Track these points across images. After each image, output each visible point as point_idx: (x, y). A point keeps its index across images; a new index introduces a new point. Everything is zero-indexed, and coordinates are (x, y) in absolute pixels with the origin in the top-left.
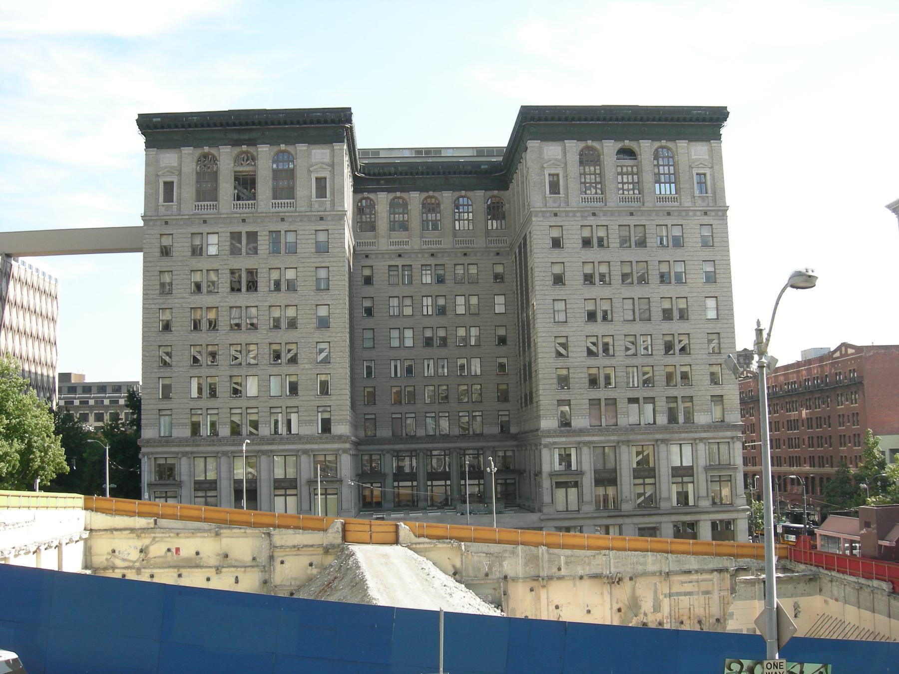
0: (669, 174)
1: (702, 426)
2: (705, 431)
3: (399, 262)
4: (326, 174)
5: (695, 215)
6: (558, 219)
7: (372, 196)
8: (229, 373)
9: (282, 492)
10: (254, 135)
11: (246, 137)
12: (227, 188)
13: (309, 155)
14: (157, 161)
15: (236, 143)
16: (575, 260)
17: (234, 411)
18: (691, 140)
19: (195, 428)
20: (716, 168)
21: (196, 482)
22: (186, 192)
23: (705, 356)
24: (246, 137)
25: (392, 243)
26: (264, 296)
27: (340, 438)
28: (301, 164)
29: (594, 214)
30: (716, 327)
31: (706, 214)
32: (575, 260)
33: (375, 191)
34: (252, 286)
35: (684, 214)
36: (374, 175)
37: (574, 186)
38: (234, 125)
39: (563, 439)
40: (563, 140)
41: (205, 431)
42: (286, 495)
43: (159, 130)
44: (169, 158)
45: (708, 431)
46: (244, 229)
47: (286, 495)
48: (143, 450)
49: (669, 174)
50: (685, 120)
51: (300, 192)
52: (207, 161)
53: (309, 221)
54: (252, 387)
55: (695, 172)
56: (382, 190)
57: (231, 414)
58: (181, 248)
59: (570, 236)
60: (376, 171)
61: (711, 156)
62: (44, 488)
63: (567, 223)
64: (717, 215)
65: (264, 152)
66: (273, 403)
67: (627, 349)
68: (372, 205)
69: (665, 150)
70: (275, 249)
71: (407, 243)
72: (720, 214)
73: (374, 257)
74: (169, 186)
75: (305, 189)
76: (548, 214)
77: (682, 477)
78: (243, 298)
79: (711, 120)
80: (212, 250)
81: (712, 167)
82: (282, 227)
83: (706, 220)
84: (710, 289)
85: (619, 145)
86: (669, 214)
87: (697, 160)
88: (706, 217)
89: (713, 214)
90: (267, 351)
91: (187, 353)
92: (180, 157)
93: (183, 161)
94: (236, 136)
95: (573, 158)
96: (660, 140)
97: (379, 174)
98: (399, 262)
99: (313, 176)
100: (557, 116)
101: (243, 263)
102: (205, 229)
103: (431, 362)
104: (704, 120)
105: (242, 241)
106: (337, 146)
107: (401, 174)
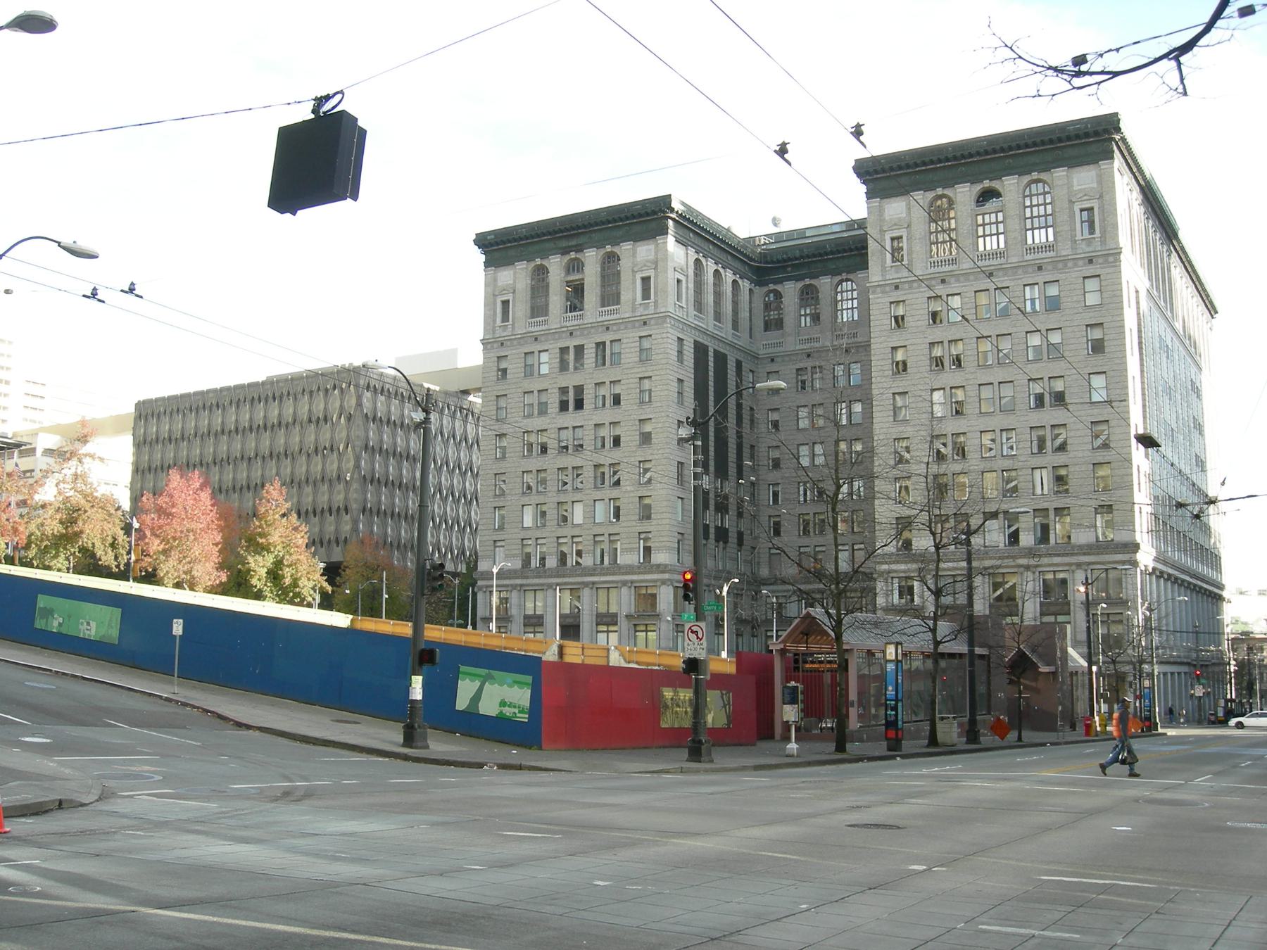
0: (1046, 215)
1: (1080, 547)
2: (1085, 554)
3: (809, 364)
4: (651, 273)
5: (1076, 265)
6: (899, 292)
7: (779, 287)
8: (556, 500)
9: (605, 628)
10: (582, 240)
11: (574, 243)
12: (556, 300)
13: (634, 255)
14: (495, 280)
15: (565, 252)
16: (919, 341)
17: (561, 540)
18: (1071, 167)
19: (527, 560)
20: (1106, 197)
21: (526, 617)
22: (520, 309)
23: (1087, 453)
24: (574, 243)
25: (802, 342)
26: (589, 416)
27: (661, 568)
28: (625, 265)
29: (943, 281)
30: (1105, 413)
31: (1091, 261)
32: (919, 341)
33: (780, 281)
34: (579, 405)
35: (1060, 265)
36: (779, 262)
37: (919, 249)
38: (562, 231)
39: (903, 567)
40: (907, 193)
41: (535, 563)
42: (608, 632)
43: (500, 247)
44: (506, 276)
45: (1089, 554)
46: (571, 343)
47: (647, 631)
48: (480, 583)
49: (1046, 215)
50: (1060, 140)
51: (625, 297)
52: (541, 272)
53: (634, 327)
54: (578, 515)
55: (1077, 208)
56: (789, 279)
57: (559, 544)
58: (514, 366)
59: (914, 313)
60: (780, 257)
61: (1100, 182)
62: (135, 580)
63: (910, 296)
64: (1106, 261)
65: (592, 258)
66: (597, 531)
67: (908, 449)
68: (778, 296)
69: (1040, 185)
70: (601, 361)
71: (817, 340)
72: (1111, 259)
73: (779, 360)
74: (505, 303)
75: (630, 290)
76: (888, 289)
77: (1056, 614)
78: (572, 418)
79: (1096, 133)
80: (545, 369)
81: (1101, 197)
82: (607, 337)
83: (1091, 270)
84: (1098, 362)
85: (978, 188)
86: (1040, 268)
87: (1080, 190)
88: (1091, 267)
89: (1101, 260)
90: (592, 474)
91: (519, 480)
92: (515, 274)
93: (517, 276)
94: (564, 244)
95: (919, 216)
96: (1029, 173)
97: (785, 261)
98: (809, 364)
99: (639, 276)
100: (887, 167)
101: (570, 380)
102: (535, 347)
103: (1038, 491)
104: (1087, 135)
105: (570, 357)
106: (660, 239)
107: (808, 257)
